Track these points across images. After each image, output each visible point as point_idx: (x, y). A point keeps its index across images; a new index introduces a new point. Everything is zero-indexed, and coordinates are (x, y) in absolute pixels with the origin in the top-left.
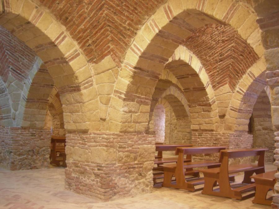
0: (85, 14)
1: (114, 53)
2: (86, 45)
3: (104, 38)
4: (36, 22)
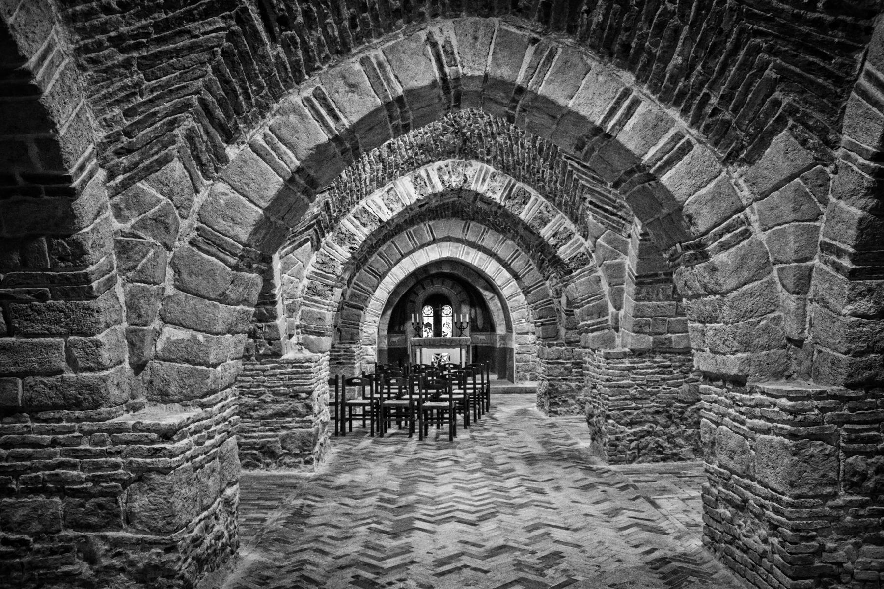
0: (672, 18)
2: (706, 114)
4: (539, 84)
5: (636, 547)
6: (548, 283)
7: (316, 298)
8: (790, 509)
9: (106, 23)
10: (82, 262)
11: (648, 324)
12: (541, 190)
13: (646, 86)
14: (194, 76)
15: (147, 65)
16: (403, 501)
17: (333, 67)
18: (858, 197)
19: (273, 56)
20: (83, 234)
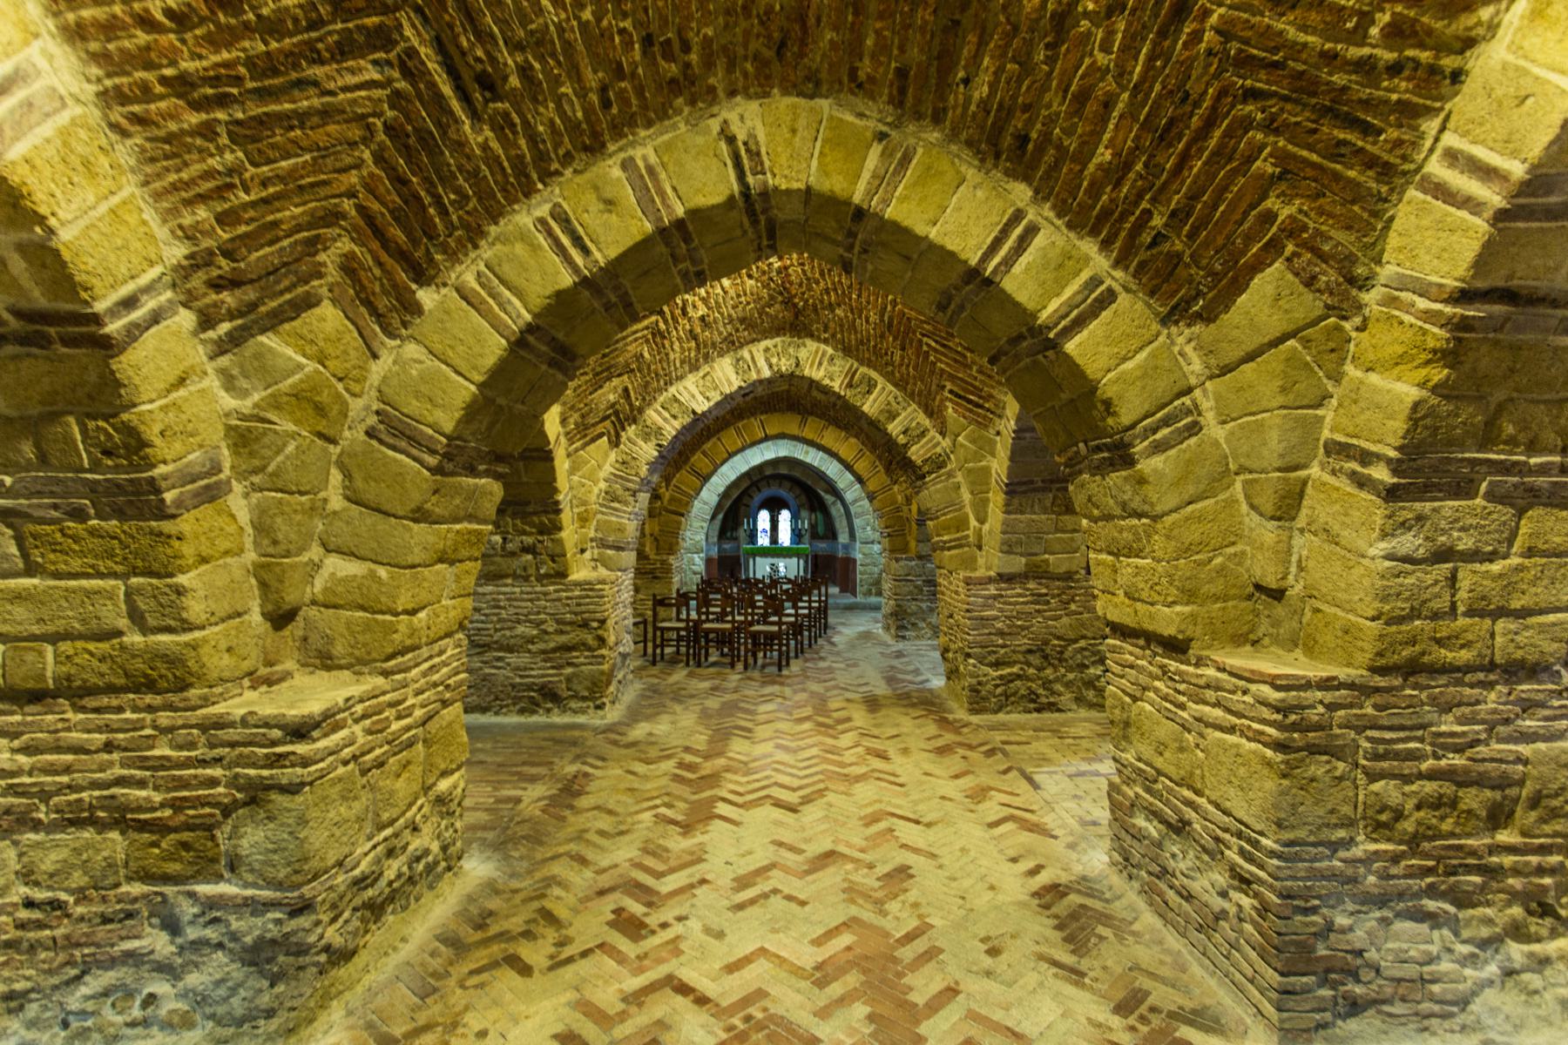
0: (1102, 79)
1: (1304, 245)
3: (1235, 173)
4: (886, 202)
5: (1014, 860)
6: (896, 488)
8: (1275, 862)
9: (148, 48)
10: (142, 458)
12: (889, 377)
14: (338, 165)
16: (708, 767)
18: (1410, 366)
19: (478, 145)
20: (140, 414)
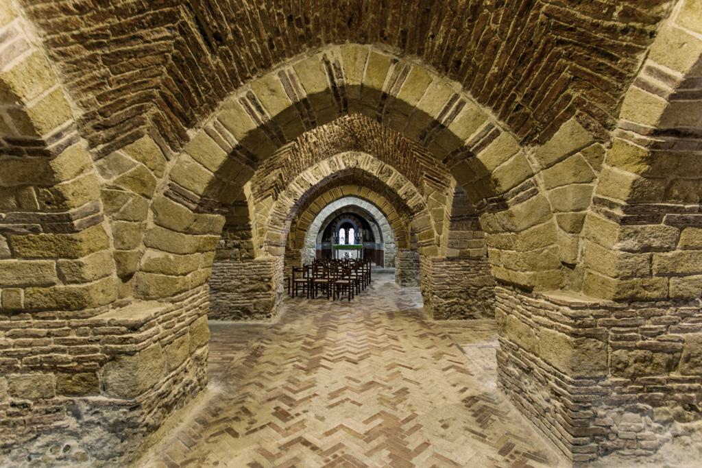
0: (494, 36)
3: (553, 77)
4: (397, 91)
5: (454, 385)
6: (401, 219)
7: (276, 226)
8: (571, 386)
9: (66, 22)
11: (457, 243)
12: (398, 169)
13: (469, 92)
15: (110, 60)
16: (317, 344)
17: (260, 77)
20: (63, 186)
